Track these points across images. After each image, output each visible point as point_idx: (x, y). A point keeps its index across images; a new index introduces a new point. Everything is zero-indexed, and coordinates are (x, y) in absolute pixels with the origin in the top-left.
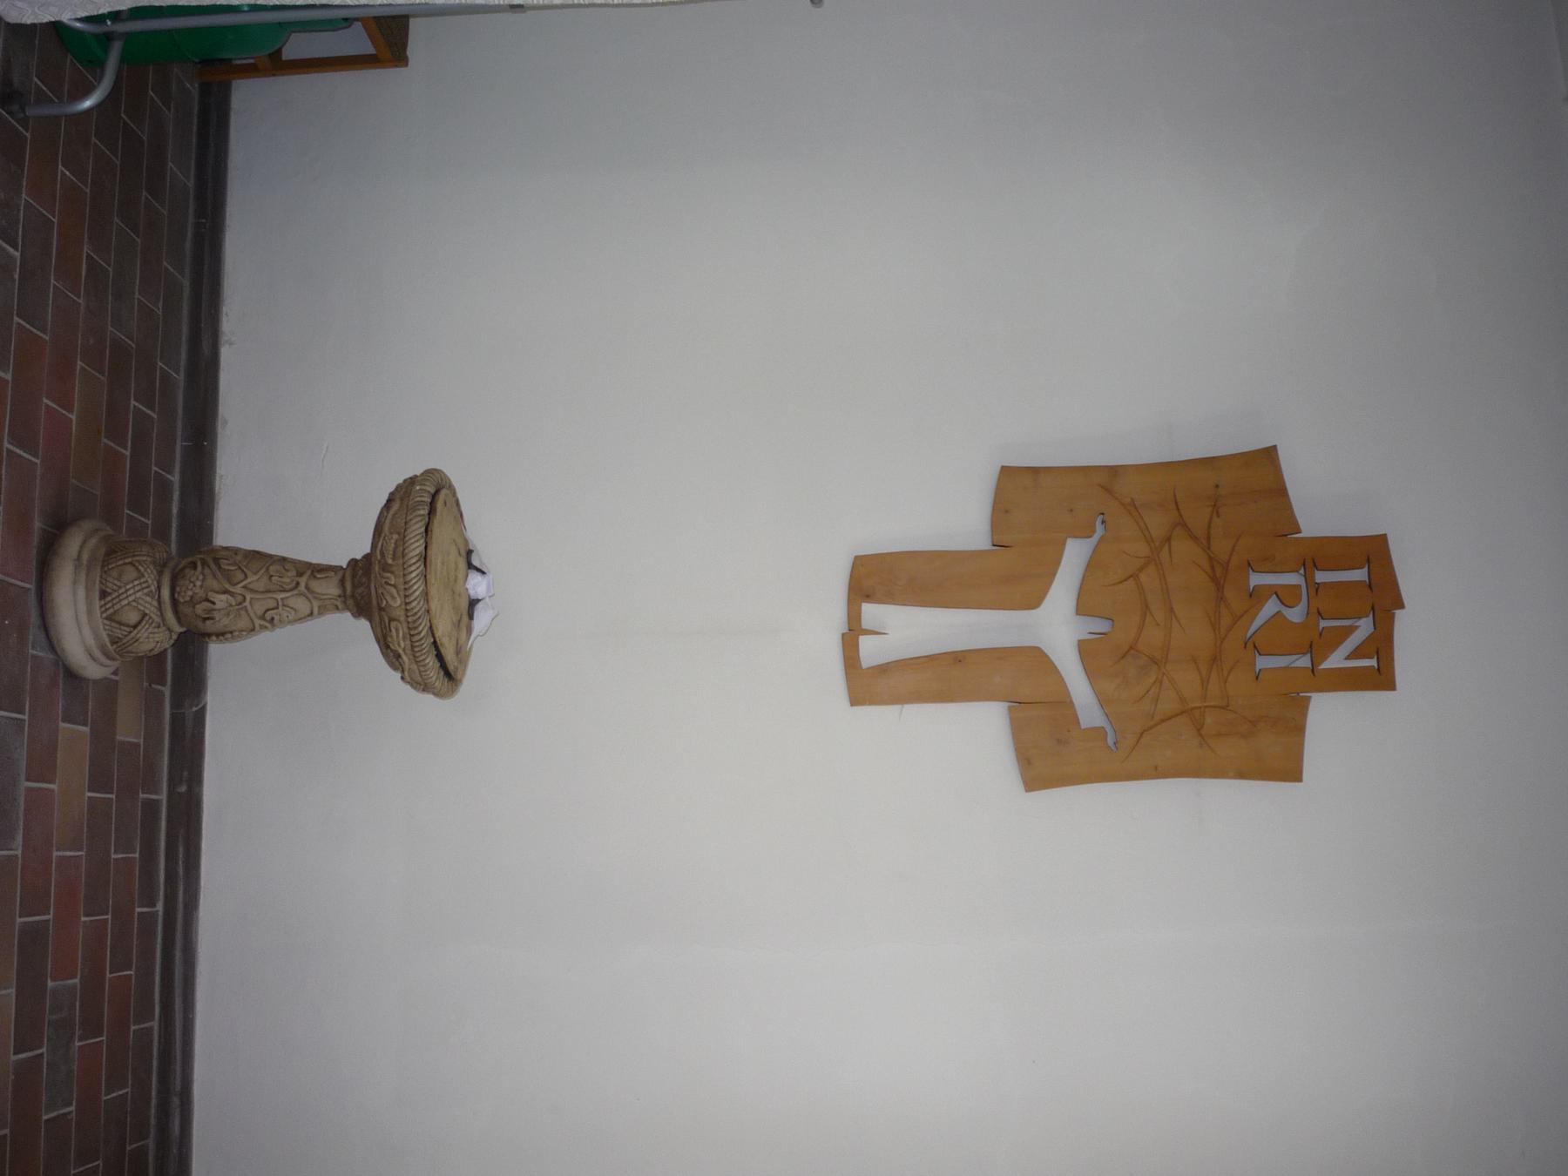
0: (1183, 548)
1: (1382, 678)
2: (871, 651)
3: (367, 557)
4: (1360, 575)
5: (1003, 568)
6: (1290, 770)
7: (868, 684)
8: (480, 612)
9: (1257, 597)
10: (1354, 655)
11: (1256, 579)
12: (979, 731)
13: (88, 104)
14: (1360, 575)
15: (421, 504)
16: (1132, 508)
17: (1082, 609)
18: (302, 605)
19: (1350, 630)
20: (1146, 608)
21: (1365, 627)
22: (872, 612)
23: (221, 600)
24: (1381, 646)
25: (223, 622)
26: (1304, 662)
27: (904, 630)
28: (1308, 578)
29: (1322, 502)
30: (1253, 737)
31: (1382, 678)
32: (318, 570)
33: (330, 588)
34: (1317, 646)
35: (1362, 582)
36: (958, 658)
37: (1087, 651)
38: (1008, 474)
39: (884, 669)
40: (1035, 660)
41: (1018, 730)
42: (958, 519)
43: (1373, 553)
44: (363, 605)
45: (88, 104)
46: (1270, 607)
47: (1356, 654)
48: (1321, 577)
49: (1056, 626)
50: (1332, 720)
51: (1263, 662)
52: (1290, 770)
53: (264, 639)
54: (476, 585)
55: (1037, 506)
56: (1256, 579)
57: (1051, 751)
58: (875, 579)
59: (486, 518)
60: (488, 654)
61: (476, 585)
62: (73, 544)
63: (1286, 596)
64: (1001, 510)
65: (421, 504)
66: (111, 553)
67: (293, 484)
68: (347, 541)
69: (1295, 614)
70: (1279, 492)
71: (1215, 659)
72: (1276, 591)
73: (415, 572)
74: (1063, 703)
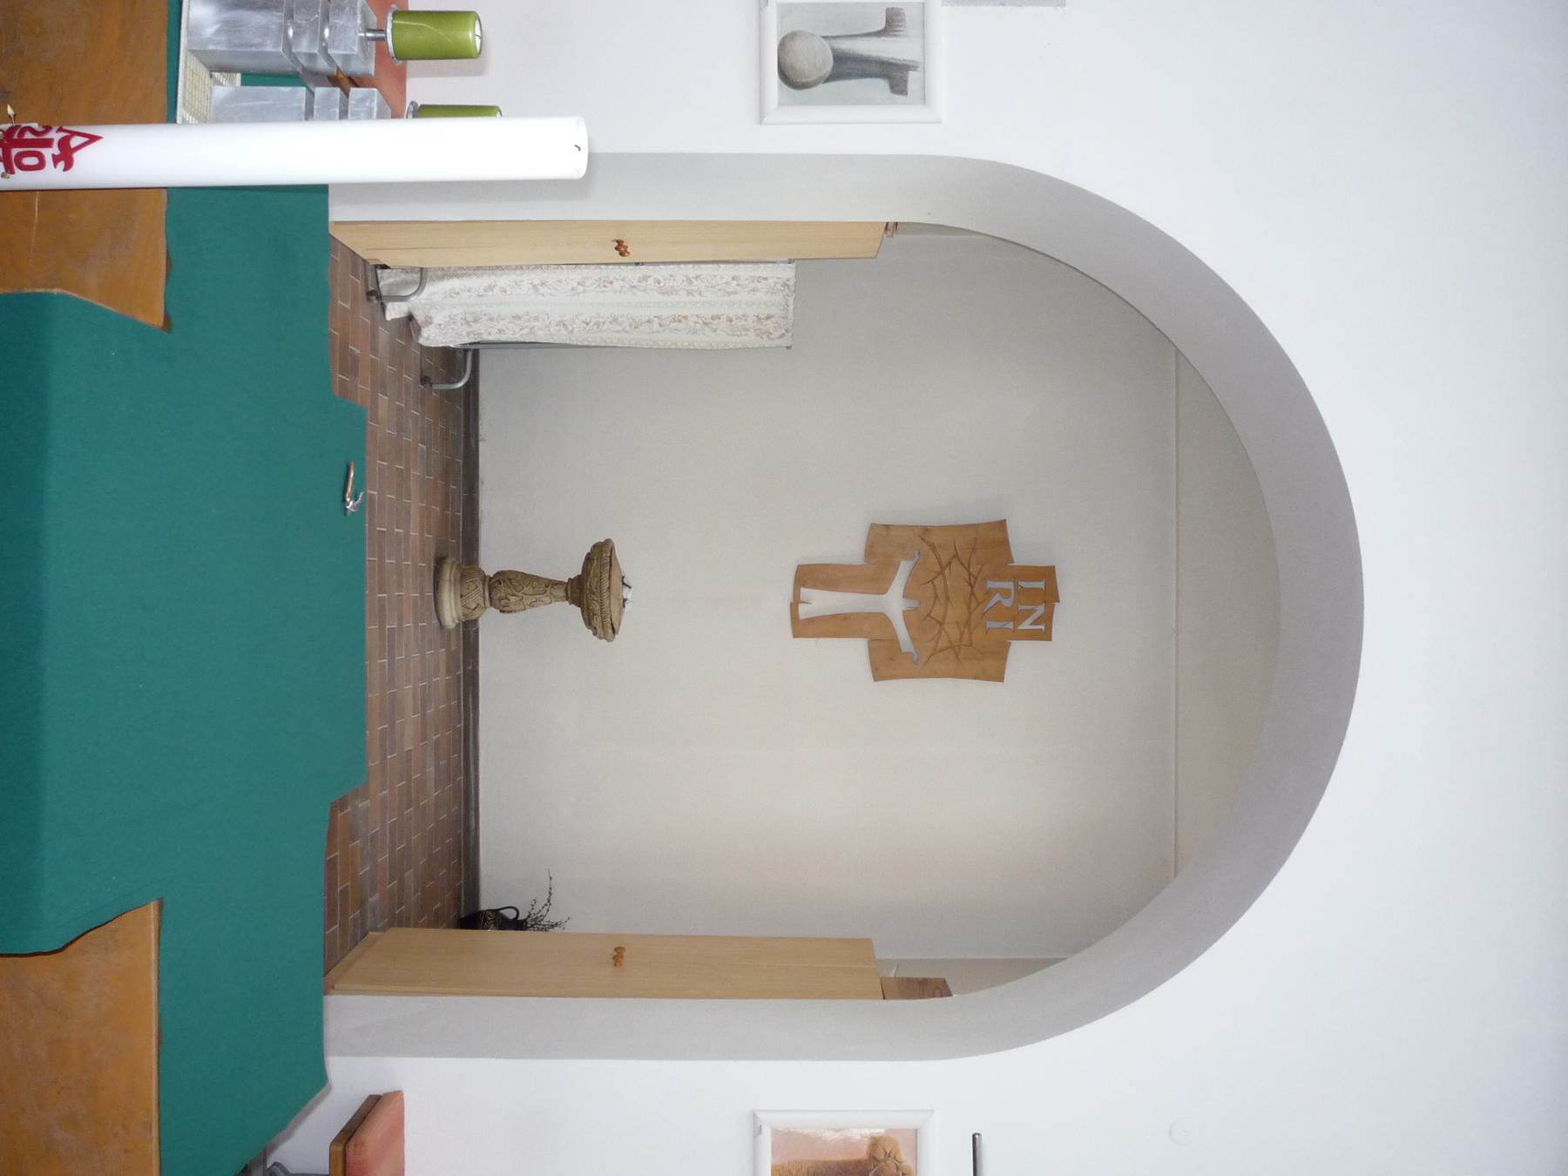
0: (957, 568)
1: (1046, 636)
2: (804, 611)
3: (579, 578)
4: (1041, 585)
5: (872, 571)
6: (999, 676)
7: (803, 627)
8: (628, 605)
9: (989, 593)
10: (1035, 622)
11: (991, 584)
12: (853, 652)
13: (460, 385)
14: (1041, 585)
15: (601, 556)
16: (932, 547)
17: (907, 595)
18: (547, 600)
19: (1032, 611)
20: (936, 597)
21: (1040, 610)
22: (805, 592)
23: (513, 599)
24: (1047, 619)
25: (512, 607)
26: (1010, 625)
27: (820, 602)
28: (1016, 586)
29: (1025, 549)
30: (987, 662)
31: (1046, 636)
32: (555, 584)
33: (561, 593)
34: (1018, 618)
35: (1039, 593)
36: (845, 617)
37: (906, 615)
38: (873, 526)
39: (811, 621)
40: (882, 620)
41: (872, 651)
42: (847, 547)
43: (1048, 574)
44: (577, 601)
45: (460, 385)
46: (997, 598)
47: (1035, 622)
48: (1022, 584)
49: (893, 603)
50: (1021, 654)
51: (991, 625)
52: (999, 676)
53: (529, 611)
54: (626, 593)
55: (886, 544)
56: (991, 584)
57: (887, 662)
58: (807, 576)
59: (625, 559)
60: (631, 620)
61: (626, 593)
62: (448, 573)
63: (1005, 594)
64: (870, 550)
65: (601, 556)
66: (462, 576)
67: (523, 525)
68: (571, 568)
69: (1008, 603)
70: (1004, 543)
71: (968, 622)
72: (998, 590)
73: (606, 596)
74: (894, 641)
